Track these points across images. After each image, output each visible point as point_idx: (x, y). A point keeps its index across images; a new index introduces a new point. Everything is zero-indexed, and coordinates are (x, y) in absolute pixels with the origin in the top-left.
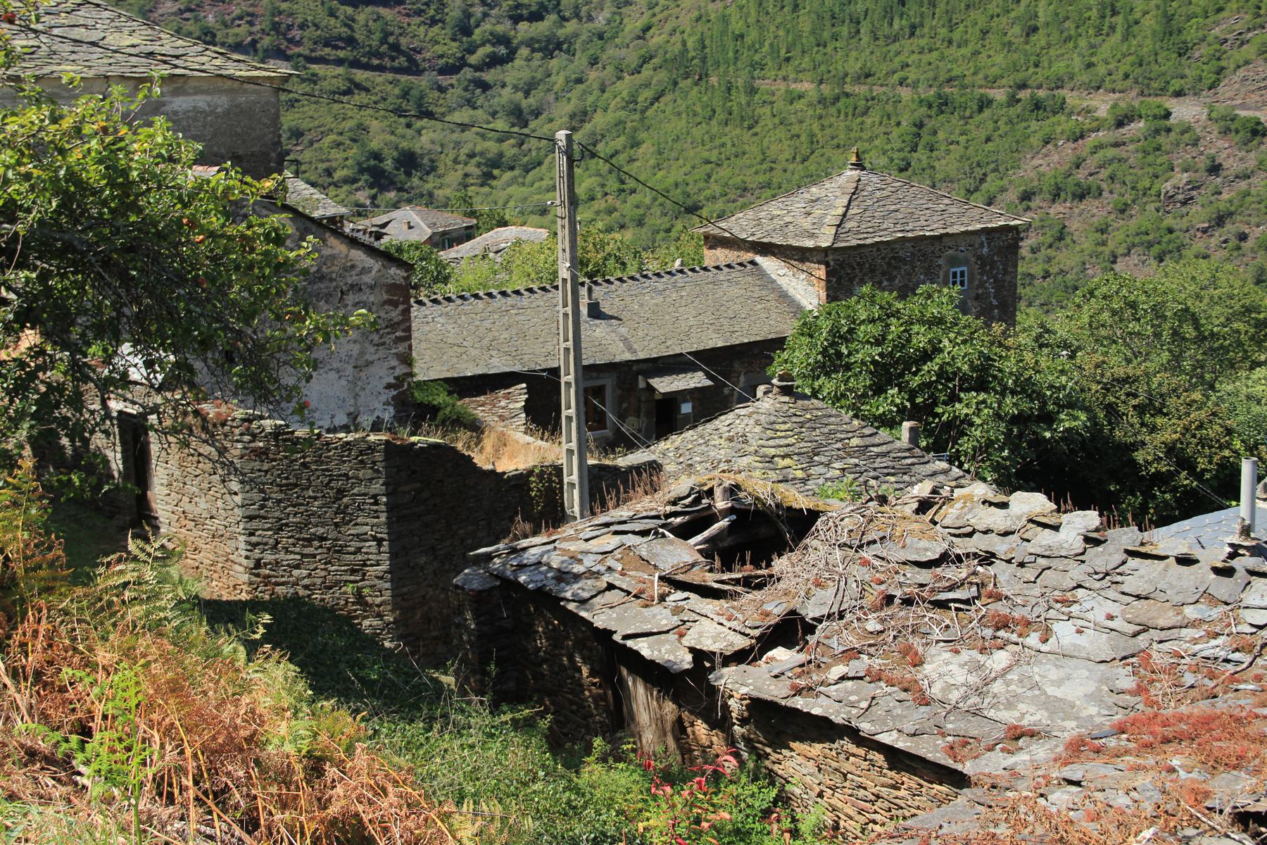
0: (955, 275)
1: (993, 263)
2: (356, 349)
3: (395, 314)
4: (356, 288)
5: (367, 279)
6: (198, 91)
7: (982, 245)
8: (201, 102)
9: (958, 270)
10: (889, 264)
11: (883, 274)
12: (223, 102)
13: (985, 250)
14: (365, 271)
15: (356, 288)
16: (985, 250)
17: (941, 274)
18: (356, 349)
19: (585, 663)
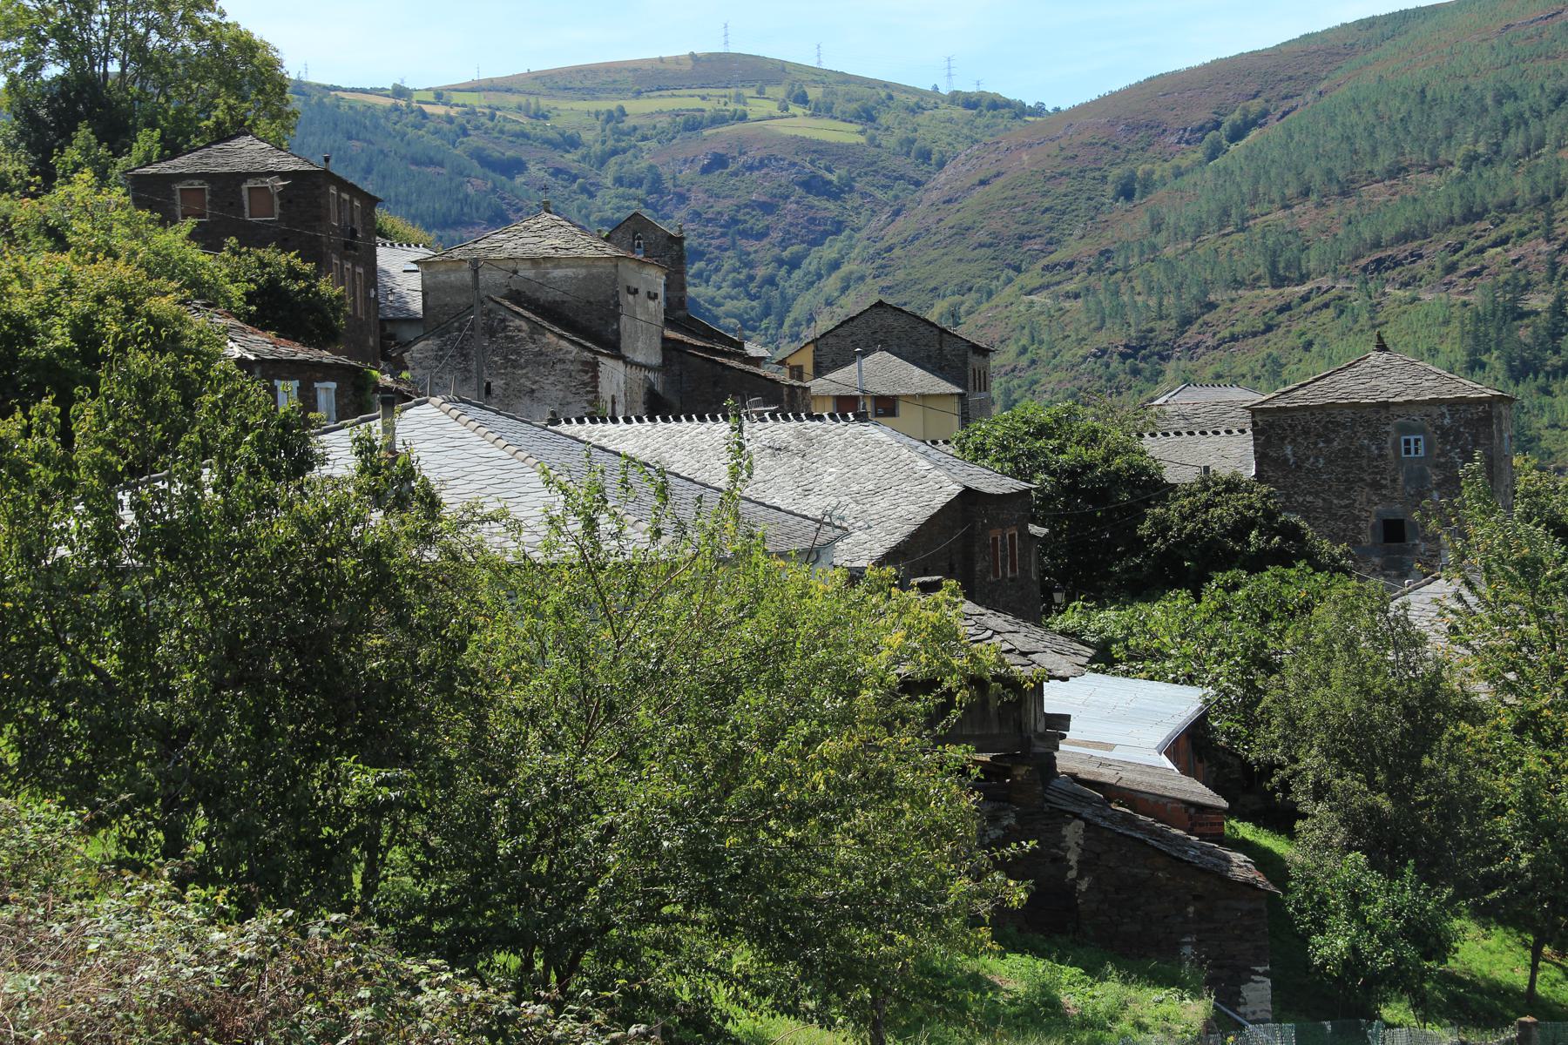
0: (1407, 442)
1: (1458, 436)
2: (561, 394)
3: (586, 378)
4: (562, 361)
5: (570, 357)
6: (568, 266)
7: (1443, 415)
8: (570, 272)
9: (1412, 438)
10: (1325, 427)
11: (1319, 436)
12: (582, 272)
13: (1447, 421)
14: (568, 352)
15: (562, 361)
16: (1447, 421)
17: (1390, 441)
18: (561, 394)
19: (1249, 886)
